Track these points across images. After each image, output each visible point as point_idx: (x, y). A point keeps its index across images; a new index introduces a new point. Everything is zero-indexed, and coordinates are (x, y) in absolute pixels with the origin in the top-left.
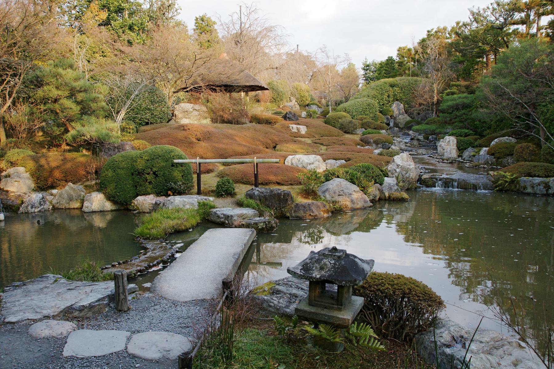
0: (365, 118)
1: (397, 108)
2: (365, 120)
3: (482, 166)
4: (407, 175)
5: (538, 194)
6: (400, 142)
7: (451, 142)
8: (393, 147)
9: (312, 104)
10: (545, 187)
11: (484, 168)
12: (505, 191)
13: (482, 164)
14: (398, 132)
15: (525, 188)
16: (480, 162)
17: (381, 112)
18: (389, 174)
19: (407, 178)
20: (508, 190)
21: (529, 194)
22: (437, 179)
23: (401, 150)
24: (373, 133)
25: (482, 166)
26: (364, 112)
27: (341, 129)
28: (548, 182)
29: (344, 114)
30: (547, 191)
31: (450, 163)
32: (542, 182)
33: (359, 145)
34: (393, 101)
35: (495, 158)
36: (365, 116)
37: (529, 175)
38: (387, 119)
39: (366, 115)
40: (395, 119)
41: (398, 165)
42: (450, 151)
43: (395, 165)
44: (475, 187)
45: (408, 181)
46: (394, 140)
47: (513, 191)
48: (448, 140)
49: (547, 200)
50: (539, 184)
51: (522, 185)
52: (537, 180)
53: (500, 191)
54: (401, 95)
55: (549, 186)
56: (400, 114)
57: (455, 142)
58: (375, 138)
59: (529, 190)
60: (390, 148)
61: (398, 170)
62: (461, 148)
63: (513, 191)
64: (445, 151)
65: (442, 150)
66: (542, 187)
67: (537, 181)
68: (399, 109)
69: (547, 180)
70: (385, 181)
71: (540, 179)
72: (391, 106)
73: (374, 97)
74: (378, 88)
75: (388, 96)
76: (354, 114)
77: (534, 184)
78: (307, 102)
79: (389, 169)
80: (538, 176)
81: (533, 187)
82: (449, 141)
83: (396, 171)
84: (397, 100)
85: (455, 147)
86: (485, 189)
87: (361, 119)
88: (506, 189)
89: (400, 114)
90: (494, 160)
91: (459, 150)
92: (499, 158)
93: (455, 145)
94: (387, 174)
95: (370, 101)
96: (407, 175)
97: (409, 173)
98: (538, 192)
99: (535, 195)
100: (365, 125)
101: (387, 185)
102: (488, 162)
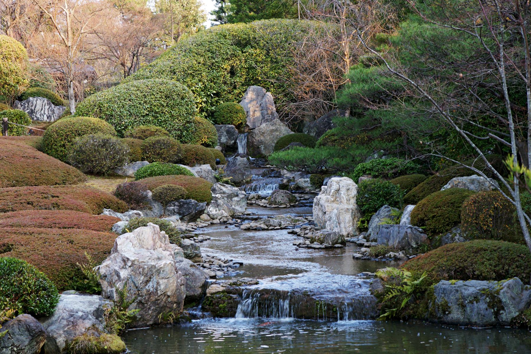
0: (152, 134)
1: (254, 104)
2: (153, 139)
3: (392, 254)
4: (150, 286)
5: (476, 324)
6: (230, 197)
7: (343, 192)
8: (212, 210)
9: (33, 95)
10: (491, 305)
11: (396, 259)
12: (404, 319)
13: (393, 249)
14: (246, 168)
15: (446, 309)
16: (391, 243)
17: (211, 115)
18: (105, 284)
19: (150, 294)
20: (409, 318)
21: (455, 325)
22: (240, 295)
23: (233, 217)
24: (162, 174)
25: (392, 254)
26: (154, 114)
27: (79, 163)
28: (498, 292)
29: (94, 120)
30: (497, 314)
31: (326, 248)
32: (484, 293)
33: (108, 207)
34: (247, 84)
35: (425, 231)
36: (153, 128)
37: (462, 274)
38: (229, 132)
39: (160, 124)
40: (251, 132)
41: (125, 260)
42: (338, 217)
43: (119, 260)
44: (332, 312)
45: (155, 303)
46: (214, 190)
47: (421, 319)
48: (335, 187)
49: (498, 340)
50: (476, 298)
51: (439, 301)
52: (474, 286)
53: (394, 319)
54: (266, 69)
55: (500, 301)
56: (264, 119)
57: (354, 192)
58: (159, 188)
59: (456, 315)
60: (202, 212)
61: (124, 274)
62: (366, 208)
63: (421, 319)
64: (327, 216)
65: (320, 214)
66: (483, 306)
67: (471, 290)
68: (263, 108)
69: (495, 285)
70: (60, 305)
71: (483, 284)
72: (239, 98)
73: (190, 73)
74: (201, 50)
75: (232, 73)
76: (126, 121)
77: (464, 298)
78: (22, 89)
79: (103, 271)
80: (477, 278)
81: (463, 306)
82: (338, 191)
83: (118, 276)
84: (257, 82)
85: (352, 205)
86: (354, 316)
87: (144, 135)
88: (405, 314)
89: (264, 119)
90: (424, 236)
91: (363, 213)
92: (435, 232)
93: (353, 201)
94: (98, 285)
95: (172, 84)
96: (150, 286)
97: (155, 279)
98: (474, 319)
99: (467, 326)
100: (151, 152)
101: (66, 315)
102: (409, 244)
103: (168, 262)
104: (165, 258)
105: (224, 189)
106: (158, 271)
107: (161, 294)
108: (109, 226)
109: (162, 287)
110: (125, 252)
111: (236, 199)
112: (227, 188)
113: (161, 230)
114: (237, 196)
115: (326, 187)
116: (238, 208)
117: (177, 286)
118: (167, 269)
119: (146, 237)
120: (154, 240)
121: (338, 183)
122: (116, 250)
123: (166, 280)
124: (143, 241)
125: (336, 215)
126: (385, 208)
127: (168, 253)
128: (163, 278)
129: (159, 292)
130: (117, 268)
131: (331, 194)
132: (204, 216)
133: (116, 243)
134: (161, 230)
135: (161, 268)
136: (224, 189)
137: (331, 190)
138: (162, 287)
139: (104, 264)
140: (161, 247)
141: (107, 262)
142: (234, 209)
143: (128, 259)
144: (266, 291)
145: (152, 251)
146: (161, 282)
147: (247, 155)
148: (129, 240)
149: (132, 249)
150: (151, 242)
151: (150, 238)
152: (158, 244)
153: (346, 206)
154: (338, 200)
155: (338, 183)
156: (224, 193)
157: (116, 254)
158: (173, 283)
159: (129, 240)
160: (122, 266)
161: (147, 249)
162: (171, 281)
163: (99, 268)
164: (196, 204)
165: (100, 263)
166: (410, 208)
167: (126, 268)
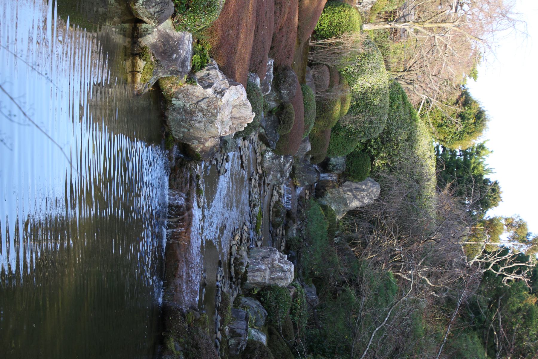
1: (362, 195)
7: (280, 274)
8: (269, 155)
41: (222, 93)
48: (286, 267)
60: (268, 145)
62: (265, 294)
82: (282, 270)
103: (219, 131)
104: (223, 128)
105: (287, 165)
106: (212, 122)
107: (191, 124)
108: (256, 67)
109: (197, 125)
110: (229, 92)
111: (279, 175)
112: (289, 167)
113: (248, 124)
114: (281, 177)
115: (286, 259)
116: (271, 177)
117: (198, 138)
118: (213, 130)
119: (242, 111)
120: (239, 118)
121: (289, 270)
122: (231, 84)
123: (203, 129)
124: (239, 109)
125: (260, 268)
126: (265, 313)
127: (228, 131)
128: (205, 126)
129: (193, 122)
130: (215, 85)
131: (279, 264)
132: (264, 147)
133: (238, 85)
134: (248, 124)
135: (214, 125)
136: (287, 165)
137: (283, 264)
138: (197, 125)
139: (219, 74)
140: (233, 124)
141: (221, 76)
142: (270, 173)
143: (223, 95)
144: (191, 216)
145: (230, 116)
146: (202, 124)
147: (319, 181)
148: (240, 96)
149: (232, 99)
150: (237, 116)
151: (241, 115)
152: (235, 122)
153: (267, 277)
154: (276, 269)
155: (289, 270)
156: (284, 165)
157: (228, 84)
158: (201, 135)
159: (240, 96)
160: (217, 89)
161: (232, 112)
162: (202, 133)
163: (216, 69)
164: (276, 140)
165: (220, 69)
166: (263, 339)
167: (215, 93)
